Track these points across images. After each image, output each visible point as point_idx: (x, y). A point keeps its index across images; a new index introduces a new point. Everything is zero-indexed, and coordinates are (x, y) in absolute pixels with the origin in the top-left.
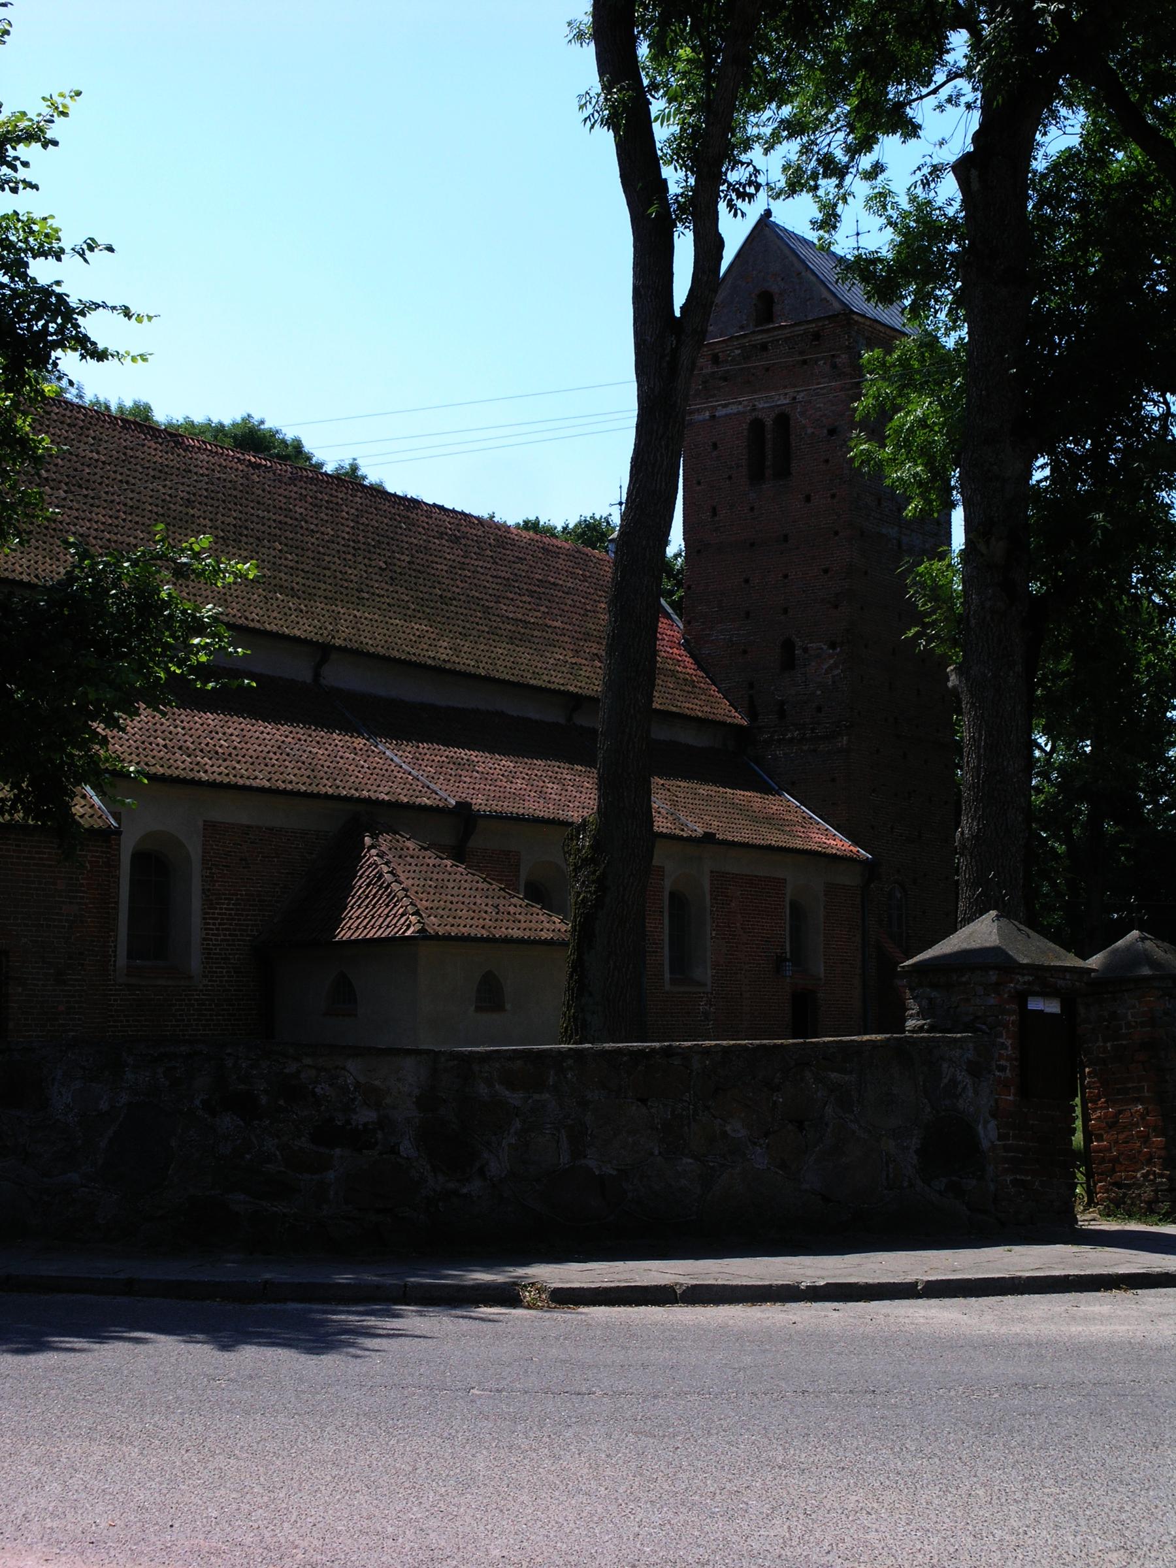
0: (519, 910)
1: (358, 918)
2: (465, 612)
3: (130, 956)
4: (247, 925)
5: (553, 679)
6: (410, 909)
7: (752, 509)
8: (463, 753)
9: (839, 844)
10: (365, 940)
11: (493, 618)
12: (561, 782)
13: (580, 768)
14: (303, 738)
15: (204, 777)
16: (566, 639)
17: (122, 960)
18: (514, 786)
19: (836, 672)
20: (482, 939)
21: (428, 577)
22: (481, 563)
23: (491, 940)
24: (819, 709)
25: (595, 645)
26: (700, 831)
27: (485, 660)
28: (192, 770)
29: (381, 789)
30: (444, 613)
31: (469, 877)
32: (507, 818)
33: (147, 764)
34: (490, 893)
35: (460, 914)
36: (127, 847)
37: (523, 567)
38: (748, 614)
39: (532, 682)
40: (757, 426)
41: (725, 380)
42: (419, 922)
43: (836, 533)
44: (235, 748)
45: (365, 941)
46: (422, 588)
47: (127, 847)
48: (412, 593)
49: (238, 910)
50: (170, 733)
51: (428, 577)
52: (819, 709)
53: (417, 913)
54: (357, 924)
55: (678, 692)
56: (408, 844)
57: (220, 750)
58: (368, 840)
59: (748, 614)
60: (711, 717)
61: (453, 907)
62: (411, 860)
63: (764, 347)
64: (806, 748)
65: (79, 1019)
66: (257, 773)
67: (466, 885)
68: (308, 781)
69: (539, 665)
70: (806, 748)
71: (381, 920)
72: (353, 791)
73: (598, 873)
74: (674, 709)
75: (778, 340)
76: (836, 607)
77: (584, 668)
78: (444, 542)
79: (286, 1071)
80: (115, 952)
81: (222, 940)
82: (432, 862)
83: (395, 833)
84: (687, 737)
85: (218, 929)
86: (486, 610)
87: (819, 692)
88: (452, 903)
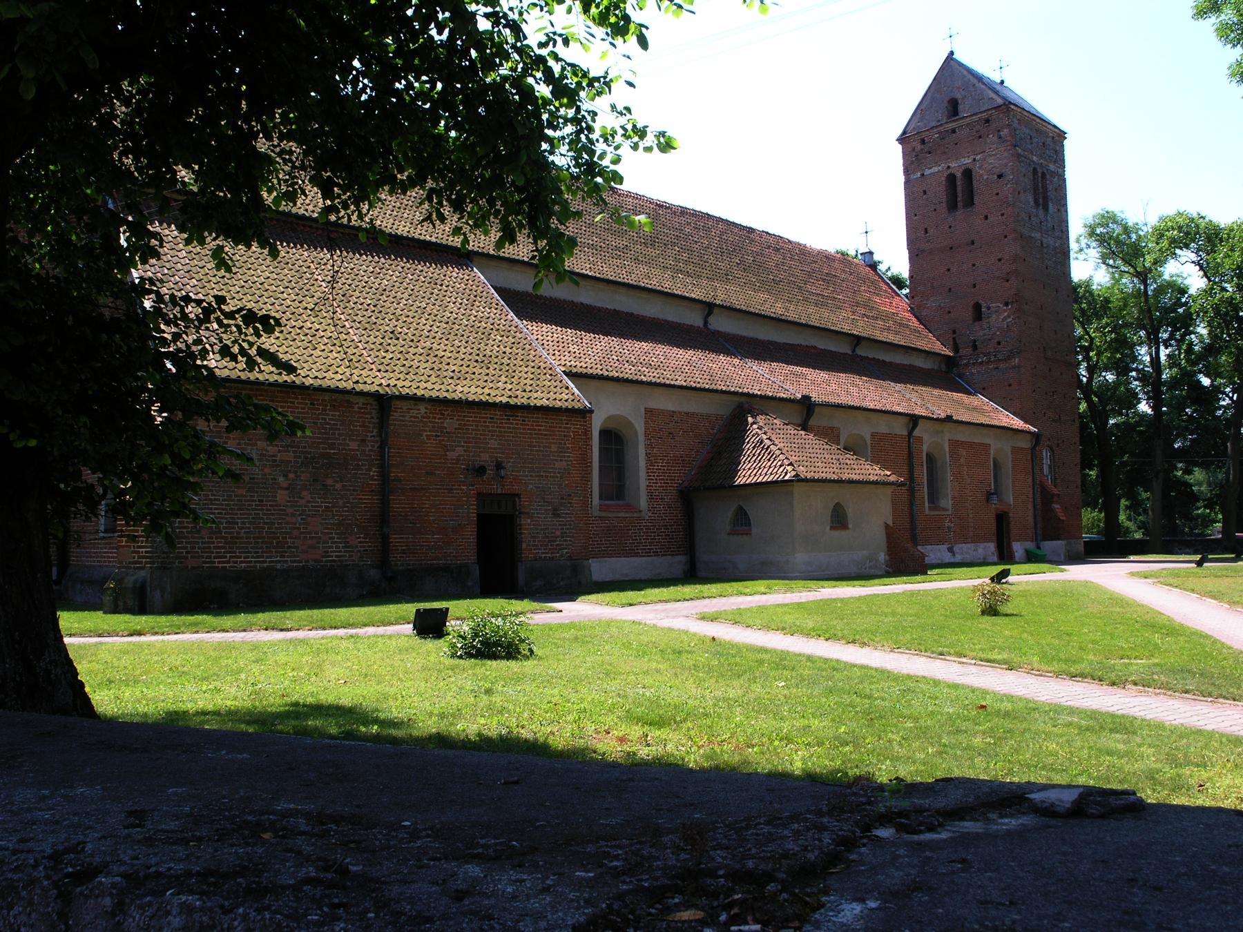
3: (601, 498)
6: (786, 462)
8: (798, 369)
9: (1017, 423)
10: (756, 484)
17: (596, 500)
20: (834, 481)
23: (840, 481)
24: (999, 343)
26: (943, 415)
36: (597, 423)
40: (951, 179)
47: (597, 423)
52: (999, 343)
54: (747, 474)
58: (750, 420)
63: (953, 131)
84: (920, 362)
86: (800, 288)
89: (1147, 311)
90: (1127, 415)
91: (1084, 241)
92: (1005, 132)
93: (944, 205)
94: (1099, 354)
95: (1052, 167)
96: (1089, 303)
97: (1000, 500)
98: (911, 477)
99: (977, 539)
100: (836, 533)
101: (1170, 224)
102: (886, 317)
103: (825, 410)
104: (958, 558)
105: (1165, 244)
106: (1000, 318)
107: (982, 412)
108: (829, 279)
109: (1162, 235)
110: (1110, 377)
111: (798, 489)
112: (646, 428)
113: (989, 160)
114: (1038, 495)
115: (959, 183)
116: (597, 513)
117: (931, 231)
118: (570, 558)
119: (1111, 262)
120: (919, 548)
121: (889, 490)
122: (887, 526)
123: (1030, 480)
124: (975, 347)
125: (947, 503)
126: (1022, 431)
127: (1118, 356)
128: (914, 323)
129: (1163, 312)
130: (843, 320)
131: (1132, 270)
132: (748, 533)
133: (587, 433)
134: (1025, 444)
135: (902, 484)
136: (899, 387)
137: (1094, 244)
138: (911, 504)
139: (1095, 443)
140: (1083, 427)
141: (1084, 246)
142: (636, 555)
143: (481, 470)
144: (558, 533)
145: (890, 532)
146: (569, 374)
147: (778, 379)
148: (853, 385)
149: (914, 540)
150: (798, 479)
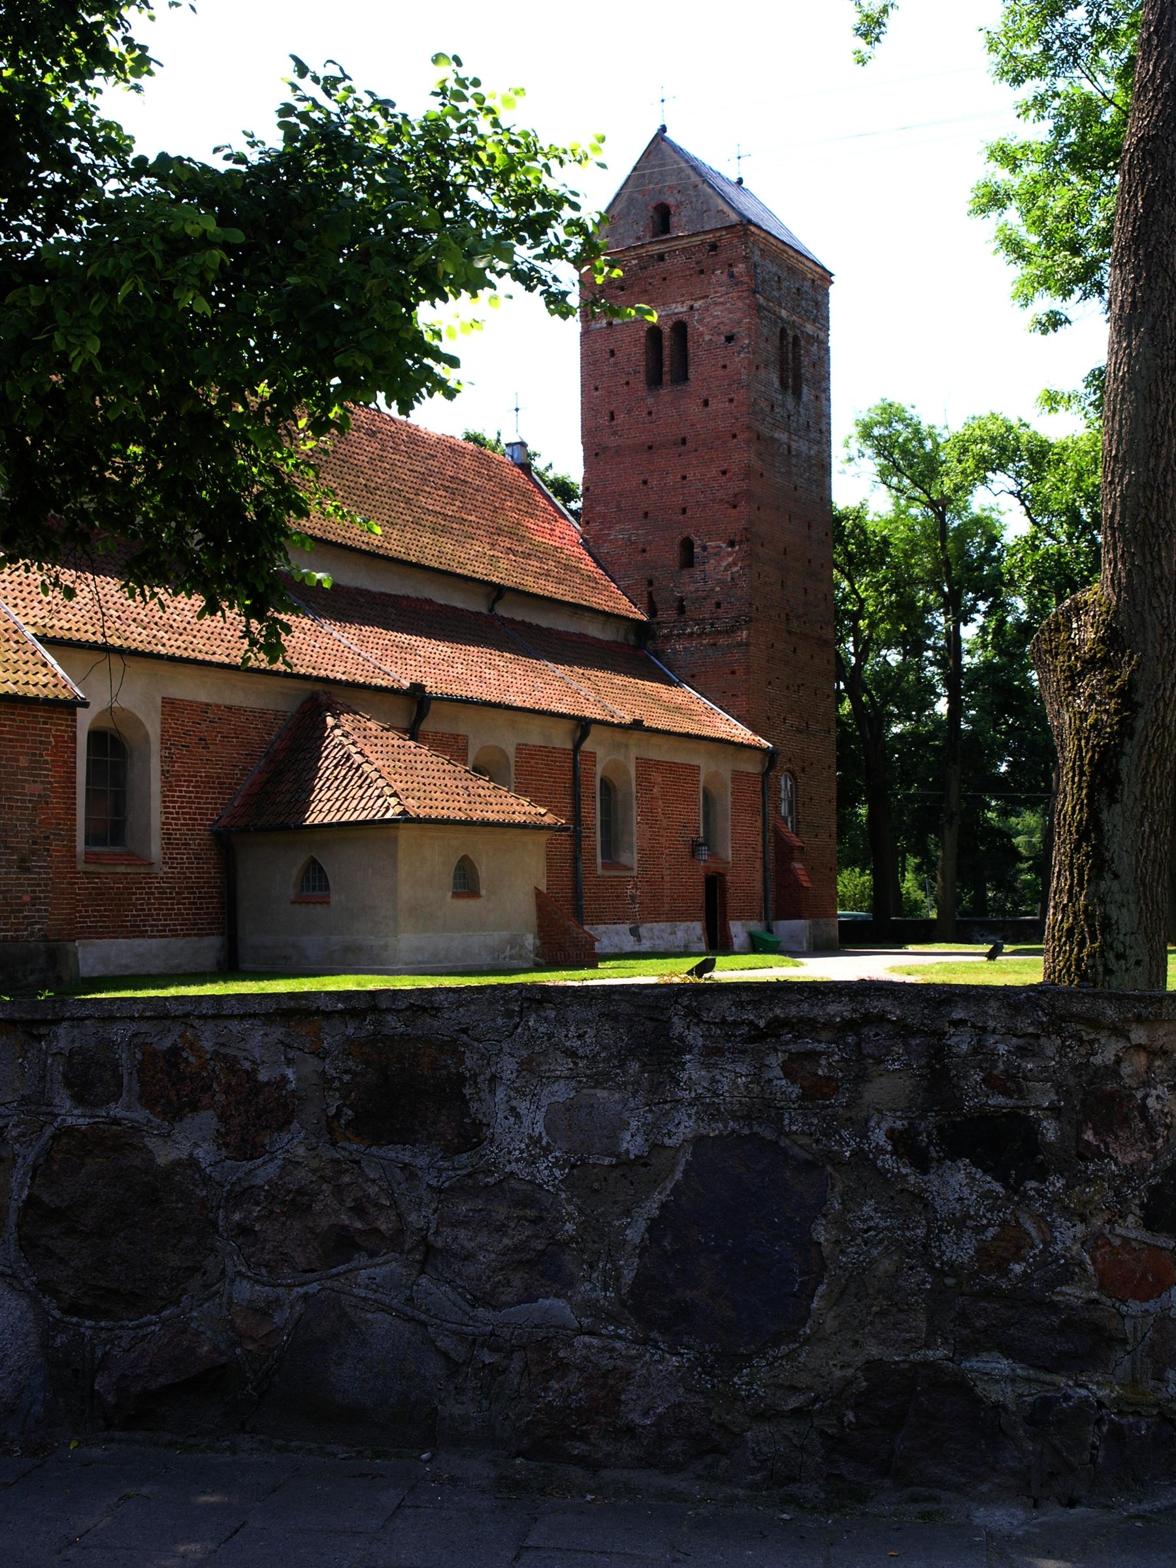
0: (488, 792)
1: (329, 800)
2: (389, 501)
3: (87, 843)
4: (207, 809)
5: (477, 569)
6: (388, 791)
7: (650, 413)
8: (404, 638)
9: (742, 733)
11: (415, 509)
15: (163, 651)
16: (482, 532)
18: (456, 671)
19: (735, 569)
20: (460, 822)
21: (351, 467)
22: (397, 457)
23: (468, 823)
24: (718, 605)
25: (507, 540)
26: (628, 719)
27: (414, 547)
28: (149, 643)
29: (336, 668)
30: (369, 501)
31: (434, 758)
32: (457, 701)
34: (457, 775)
35: (435, 796)
37: (435, 463)
38: (646, 514)
39: (458, 571)
41: (622, 289)
42: (399, 804)
43: (734, 436)
44: (189, 623)
46: (347, 477)
47: (85, 720)
48: (339, 481)
49: (197, 792)
50: (122, 604)
51: (351, 467)
52: (718, 605)
54: (325, 808)
55: (583, 587)
56: (369, 724)
57: (175, 625)
58: (330, 721)
59: (646, 514)
60: (616, 611)
61: (428, 788)
62: (376, 741)
63: (661, 257)
64: (705, 642)
65: (46, 910)
66: (214, 648)
67: (433, 766)
69: (463, 555)
70: (705, 642)
71: (355, 802)
72: (310, 670)
73: (1118, 683)
75: (675, 251)
76: (735, 507)
78: (362, 435)
79: (1097, 1060)
81: (182, 825)
82: (396, 742)
83: (356, 713)
84: (594, 630)
85: (177, 813)
86: (408, 501)
87: (718, 589)
89: (943, 567)
90: (918, 721)
91: (856, 445)
92: (740, 268)
93: (642, 377)
94: (872, 626)
95: (809, 328)
96: (859, 545)
97: (713, 855)
98: (576, 818)
99: (676, 915)
100: (462, 903)
101: (978, 432)
102: (542, 554)
103: (445, 708)
104: (646, 945)
105: (970, 464)
106: (721, 564)
107: (690, 714)
108: (455, 487)
109: (965, 451)
110: (894, 657)
111: (405, 834)
113: (715, 310)
114: (771, 847)
115: (666, 343)
116: (81, 867)
117: (621, 418)
118: (45, 939)
119: (895, 480)
120: (586, 928)
121: (544, 837)
122: (538, 893)
123: (759, 824)
124: (681, 610)
125: (631, 858)
126: (749, 747)
127: (903, 628)
128: (588, 565)
129: (962, 565)
130: (477, 558)
131: (924, 498)
132: (325, 902)
134: (752, 767)
135: (562, 829)
136: (561, 670)
137: (869, 452)
138: (576, 859)
139: (861, 758)
140: (843, 742)
141: (855, 454)
142: (142, 934)
144: (27, 898)
145: (542, 900)
146: (43, 639)
147: (373, 655)
149: (579, 914)
150: (406, 818)
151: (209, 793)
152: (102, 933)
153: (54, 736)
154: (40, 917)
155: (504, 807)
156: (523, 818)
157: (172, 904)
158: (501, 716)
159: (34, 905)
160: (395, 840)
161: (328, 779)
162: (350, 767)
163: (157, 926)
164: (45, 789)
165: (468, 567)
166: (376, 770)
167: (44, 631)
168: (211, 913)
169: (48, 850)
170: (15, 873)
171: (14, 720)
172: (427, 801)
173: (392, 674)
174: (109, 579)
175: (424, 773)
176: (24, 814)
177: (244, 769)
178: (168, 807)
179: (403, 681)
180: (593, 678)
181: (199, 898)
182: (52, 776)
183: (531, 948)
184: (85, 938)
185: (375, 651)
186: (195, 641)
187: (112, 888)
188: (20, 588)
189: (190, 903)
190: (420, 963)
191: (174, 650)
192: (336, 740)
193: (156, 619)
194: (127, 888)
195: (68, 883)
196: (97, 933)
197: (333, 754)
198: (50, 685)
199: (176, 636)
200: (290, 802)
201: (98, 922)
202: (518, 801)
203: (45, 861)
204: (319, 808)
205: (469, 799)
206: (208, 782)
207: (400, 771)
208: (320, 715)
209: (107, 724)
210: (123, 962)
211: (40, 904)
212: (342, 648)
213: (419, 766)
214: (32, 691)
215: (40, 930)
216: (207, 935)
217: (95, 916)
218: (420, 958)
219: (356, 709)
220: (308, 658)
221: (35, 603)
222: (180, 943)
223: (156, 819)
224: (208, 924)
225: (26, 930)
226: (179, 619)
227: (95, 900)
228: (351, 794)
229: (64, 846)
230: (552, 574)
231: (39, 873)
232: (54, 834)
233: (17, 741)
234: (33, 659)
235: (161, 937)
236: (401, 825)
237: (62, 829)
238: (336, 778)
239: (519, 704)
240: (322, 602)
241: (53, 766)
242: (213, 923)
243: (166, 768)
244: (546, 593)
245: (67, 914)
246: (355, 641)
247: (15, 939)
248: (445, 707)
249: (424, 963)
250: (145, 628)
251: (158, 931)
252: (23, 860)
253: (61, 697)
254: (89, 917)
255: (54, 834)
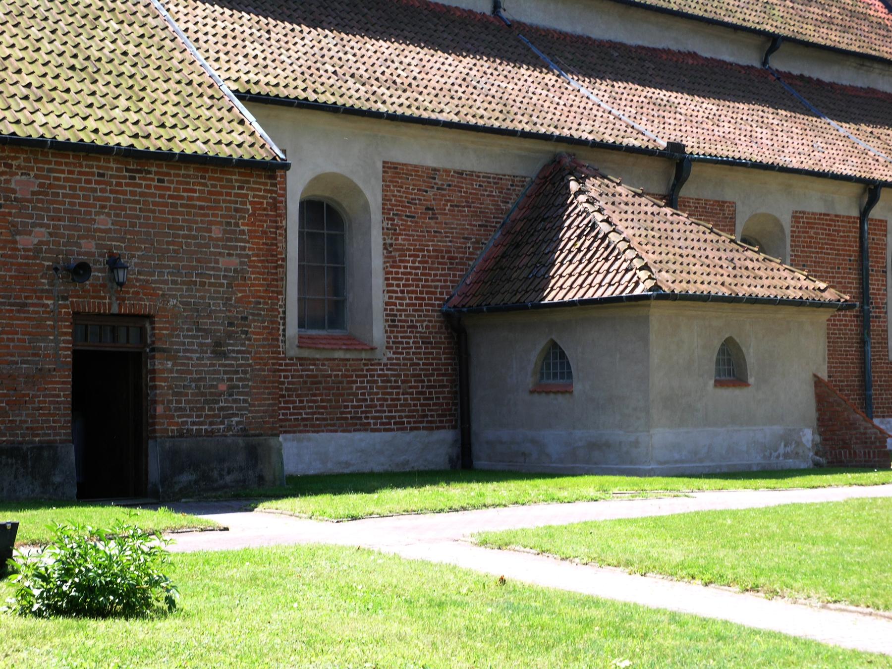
0: (756, 265)
1: (570, 275)
3: (301, 325)
5: (747, 17)
6: (637, 263)
12: (769, 126)
13: (784, 113)
14: (489, 71)
15: (383, 109)
23: (733, 300)
28: (368, 100)
29: (582, 127)
33: (315, 91)
34: (720, 245)
35: (694, 269)
36: (296, 187)
39: (726, 19)
42: (650, 278)
45: (583, 303)
47: (296, 187)
49: (425, 268)
53: (645, 267)
54: (566, 285)
57: (399, 81)
58: (574, 186)
61: (685, 260)
62: (626, 208)
65: (245, 401)
66: (442, 106)
67: (692, 236)
68: (502, 117)
71: (600, 277)
72: (552, 129)
74: (874, 53)
77: (777, 8)
80: (284, 318)
81: (407, 305)
82: (649, 209)
83: (604, 177)
85: (402, 292)
88: (681, 256)
103: (710, 171)
111: (657, 312)
112: (385, 199)
118: (244, 433)
120: (876, 421)
121: (824, 316)
122: (818, 382)
132: (567, 391)
133: (277, 207)
136: (846, 129)
138: (863, 343)
142: (365, 428)
143: (81, 271)
144: (223, 387)
146: (245, 97)
147: (626, 114)
148: (762, 124)
149: (867, 407)
150: (658, 294)
151: (438, 269)
152: (319, 426)
153: (251, 203)
154: (238, 409)
155: (776, 282)
156: (799, 294)
157: (398, 394)
158: (773, 180)
159: (231, 395)
160: (646, 320)
161: (570, 251)
162: (595, 237)
163: (381, 418)
164: (242, 263)
165: (738, 15)
166: (624, 239)
167: (248, 87)
168: (442, 404)
169: (246, 333)
170: (208, 358)
171: (205, 185)
172: (684, 274)
173: (648, 133)
174: (327, 32)
175: (682, 243)
176: (219, 292)
177: (477, 242)
178: (392, 285)
179: (659, 141)
180: (883, 137)
181: (428, 387)
182: (250, 249)
183: (809, 445)
184: (300, 432)
185: (628, 109)
186: (421, 98)
187: (330, 376)
188: (224, 41)
189: (417, 393)
190: (676, 462)
191: (395, 107)
192: (580, 208)
193: (378, 74)
194: (346, 376)
195: (269, 370)
196: (313, 426)
197: (576, 223)
198: (246, 145)
199: (400, 92)
200: (527, 278)
201: (314, 413)
202: (792, 275)
203: (243, 345)
204: (559, 284)
205: (735, 272)
206: (437, 257)
207: (653, 240)
208: (562, 179)
209: (320, 193)
210: (344, 458)
211: (239, 394)
212: (590, 105)
213: (676, 235)
214: (225, 152)
215: (238, 423)
216: (438, 428)
217: (310, 407)
218: (677, 456)
219: (605, 172)
220: (550, 116)
221: (240, 57)
222: (408, 436)
223: (378, 298)
224: (439, 416)
225: (222, 423)
226: (404, 74)
227: (310, 389)
228: (596, 268)
229: (264, 328)
230: (836, 21)
231: (236, 359)
232: (253, 314)
233: (209, 208)
234: (228, 116)
235: (385, 430)
236: (653, 303)
237: (263, 309)
238: (579, 250)
239: (795, 164)
240: (570, 57)
241: (251, 237)
242: (445, 416)
243: (389, 241)
244: (829, 43)
245: (269, 405)
246: (606, 98)
247: (210, 434)
248: (709, 169)
249: (682, 461)
250: (364, 85)
251: (382, 424)
252: (218, 344)
253: (258, 158)
254: (304, 408)
255: (253, 314)
